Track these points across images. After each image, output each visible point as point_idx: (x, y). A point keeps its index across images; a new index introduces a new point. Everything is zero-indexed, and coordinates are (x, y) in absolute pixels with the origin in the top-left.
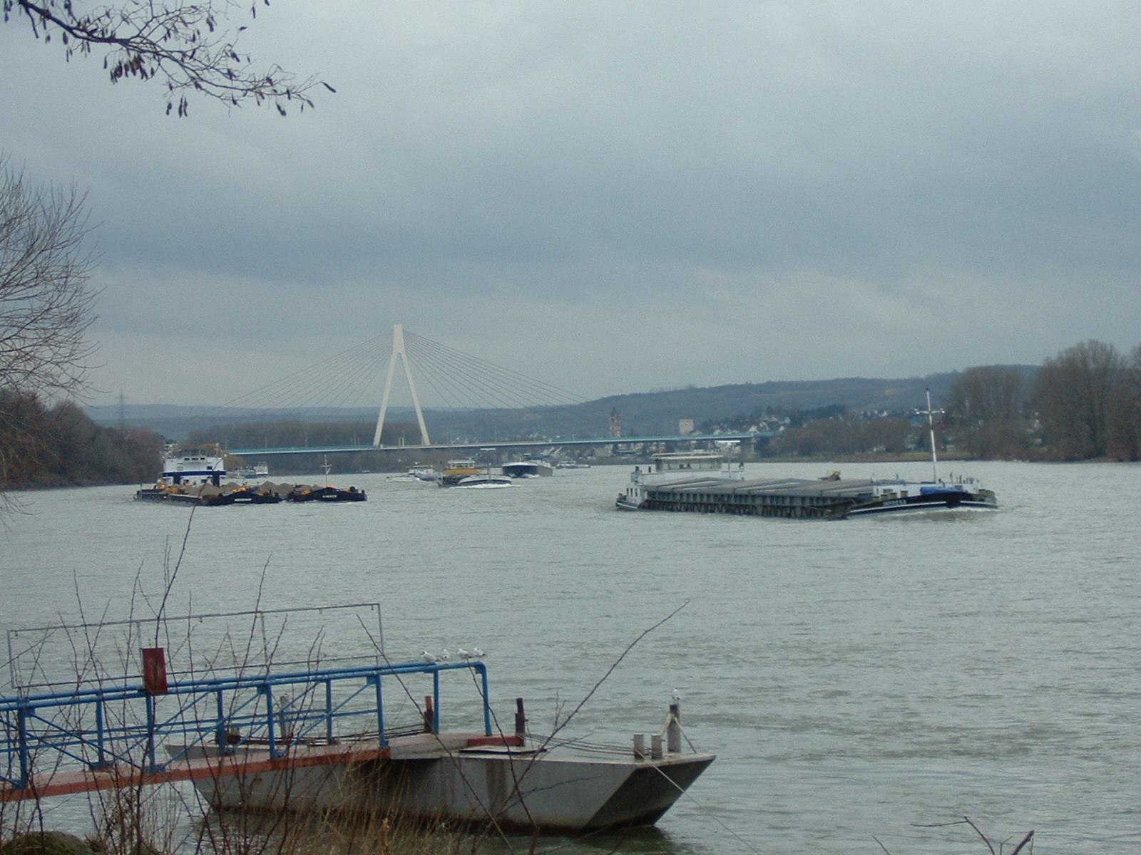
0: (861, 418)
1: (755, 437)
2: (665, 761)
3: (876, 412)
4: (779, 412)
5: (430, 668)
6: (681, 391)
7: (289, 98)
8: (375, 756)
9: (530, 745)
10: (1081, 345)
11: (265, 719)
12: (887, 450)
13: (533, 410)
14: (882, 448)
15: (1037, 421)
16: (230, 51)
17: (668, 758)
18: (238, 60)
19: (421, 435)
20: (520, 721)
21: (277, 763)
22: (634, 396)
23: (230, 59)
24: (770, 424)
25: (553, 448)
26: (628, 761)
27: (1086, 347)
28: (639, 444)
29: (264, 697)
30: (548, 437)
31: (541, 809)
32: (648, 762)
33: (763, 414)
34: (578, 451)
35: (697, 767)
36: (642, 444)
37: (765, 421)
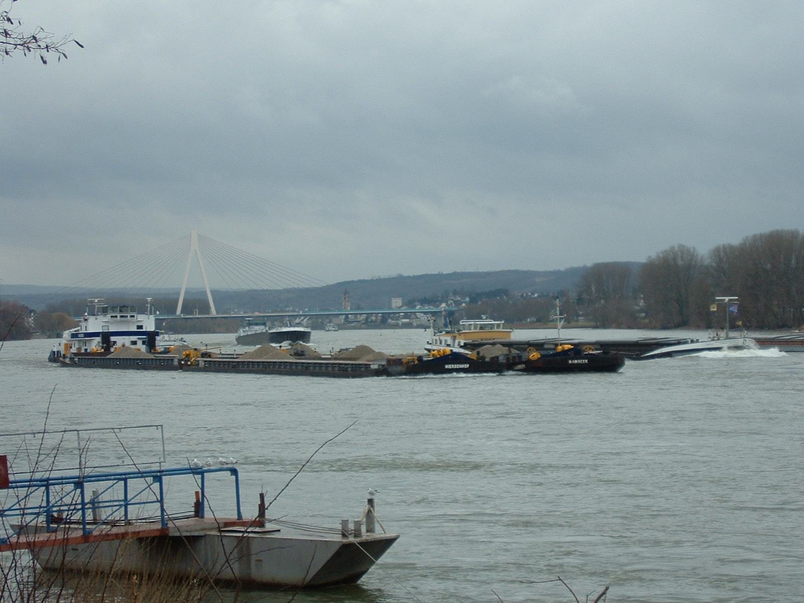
0: (519, 298)
1: (444, 311)
2: (363, 538)
3: (530, 294)
4: (463, 294)
5: (197, 471)
6: (394, 278)
7: (48, 51)
8: (158, 534)
9: (269, 526)
10: (673, 248)
11: (80, 507)
12: (537, 320)
13: (288, 291)
14: (534, 319)
15: (642, 301)
16: (6, 16)
17: (365, 536)
18: (12, 23)
19: (210, 308)
20: (262, 508)
21: (86, 537)
22: (361, 281)
23: (7, 22)
24: (455, 302)
25: (302, 318)
26: (338, 538)
27: (676, 249)
28: (363, 315)
29: (157, 484)
30: (300, 310)
31: (268, 571)
32: (351, 539)
33: (451, 294)
34: (320, 320)
35: (387, 543)
36: (365, 315)
37: (452, 300)
